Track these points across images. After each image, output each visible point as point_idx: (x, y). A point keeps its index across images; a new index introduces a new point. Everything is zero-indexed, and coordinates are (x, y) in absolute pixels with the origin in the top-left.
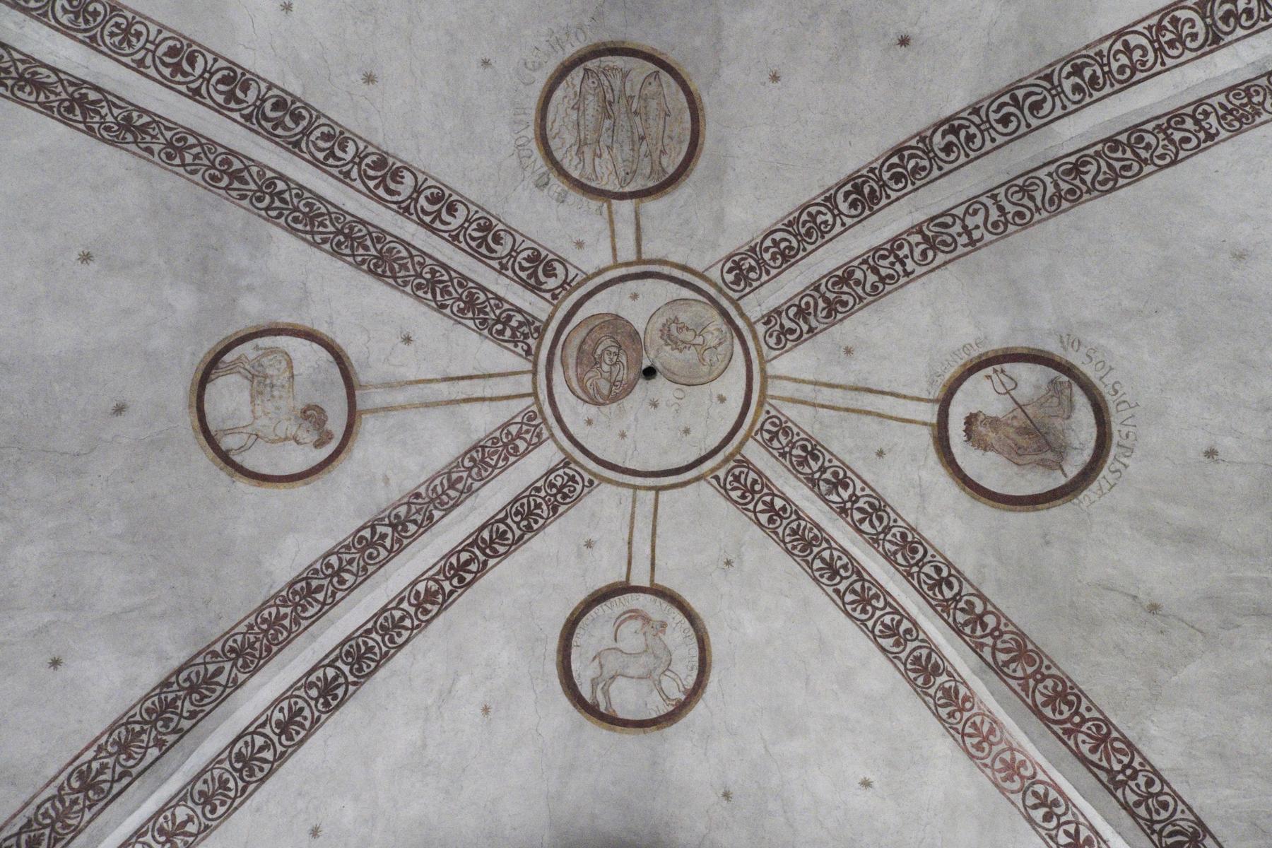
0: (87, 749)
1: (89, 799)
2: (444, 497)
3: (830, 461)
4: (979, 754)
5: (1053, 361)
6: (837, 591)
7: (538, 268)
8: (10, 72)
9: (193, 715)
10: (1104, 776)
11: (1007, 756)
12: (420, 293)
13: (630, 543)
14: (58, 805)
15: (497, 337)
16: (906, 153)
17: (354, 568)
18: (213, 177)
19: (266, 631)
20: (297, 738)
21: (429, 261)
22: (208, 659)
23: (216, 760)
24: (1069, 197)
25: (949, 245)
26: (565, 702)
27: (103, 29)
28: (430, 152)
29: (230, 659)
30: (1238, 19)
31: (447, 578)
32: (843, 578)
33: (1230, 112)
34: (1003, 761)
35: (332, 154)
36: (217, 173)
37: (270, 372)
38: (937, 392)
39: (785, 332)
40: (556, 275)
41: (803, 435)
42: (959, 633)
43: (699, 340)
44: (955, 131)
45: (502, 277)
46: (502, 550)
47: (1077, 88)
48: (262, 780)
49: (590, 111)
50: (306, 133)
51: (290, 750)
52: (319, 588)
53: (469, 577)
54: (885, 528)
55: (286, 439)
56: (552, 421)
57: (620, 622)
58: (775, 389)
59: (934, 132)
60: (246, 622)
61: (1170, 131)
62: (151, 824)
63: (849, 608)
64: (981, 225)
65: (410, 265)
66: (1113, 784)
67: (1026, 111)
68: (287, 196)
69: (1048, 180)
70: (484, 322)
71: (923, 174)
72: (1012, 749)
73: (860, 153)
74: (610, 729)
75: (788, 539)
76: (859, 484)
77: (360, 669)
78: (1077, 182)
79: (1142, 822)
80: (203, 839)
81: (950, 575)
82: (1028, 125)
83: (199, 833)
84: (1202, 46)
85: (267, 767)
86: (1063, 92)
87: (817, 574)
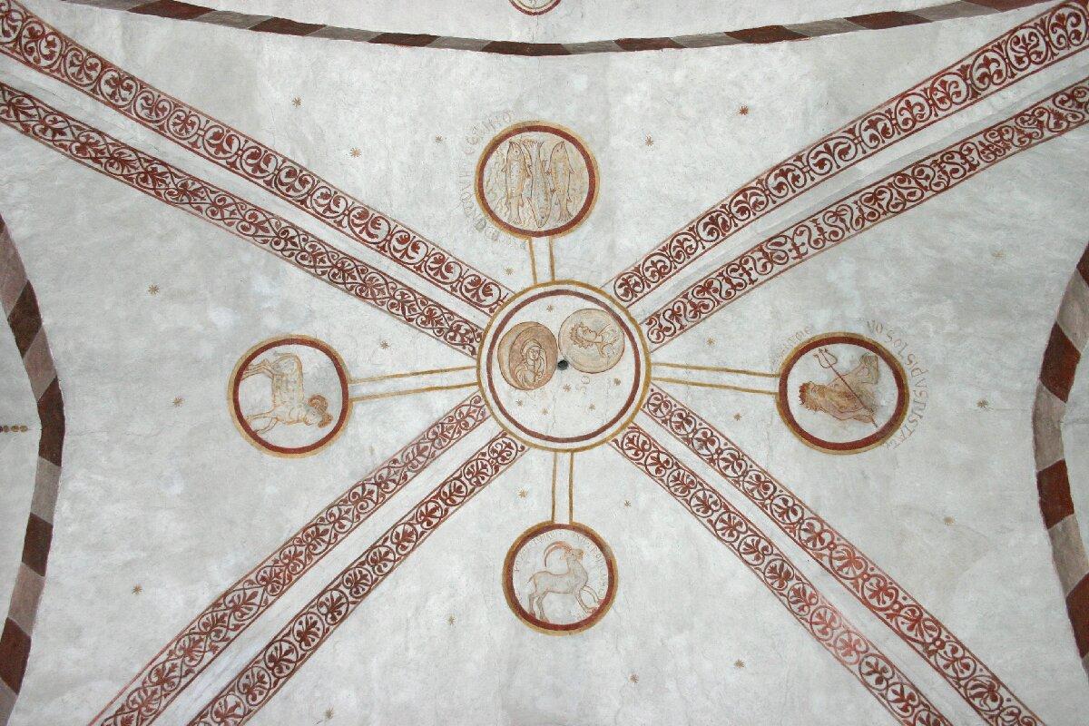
0: (162, 653)
1: (165, 690)
2: (415, 462)
3: (700, 424)
4: (826, 637)
5: (863, 341)
6: (710, 521)
7: (478, 289)
8: (103, 153)
9: (237, 627)
11: (845, 637)
12: (394, 310)
13: (553, 492)
14: (143, 694)
16: (748, 192)
17: (350, 516)
18: (244, 228)
19: (287, 565)
20: (313, 644)
21: (399, 286)
22: (246, 586)
23: (255, 661)
24: (870, 218)
25: (783, 259)
27: (168, 121)
28: (399, 208)
29: (262, 586)
30: (991, 78)
31: (418, 523)
32: (713, 511)
33: (987, 148)
34: (842, 641)
35: (329, 209)
36: (247, 225)
37: (285, 371)
38: (778, 369)
39: (662, 329)
40: (492, 295)
41: (679, 406)
42: (804, 547)
43: (599, 339)
44: (784, 174)
45: (453, 297)
46: (459, 500)
47: (873, 138)
48: (289, 676)
49: (515, 173)
50: (310, 194)
51: (308, 653)
52: (326, 532)
53: (435, 521)
54: (743, 472)
55: (298, 421)
56: (492, 403)
57: (548, 551)
59: (769, 176)
60: (273, 558)
61: (943, 165)
62: (210, 708)
63: (720, 533)
64: (806, 242)
65: (386, 290)
66: (928, 653)
67: (836, 156)
68: (296, 240)
69: (854, 207)
70: (441, 330)
71: (762, 207)
72: (848, 632)
73: (713, 196)
74: (544, 632)
75: (671, 484)
76: (723, 441)
77: (357, 592)
78: (876, 207)
79: (951, 680)
80: (248, 720)
81: (794, 505)
82: (838, 167)
83: (245, 715)
84: (965, 100)
85: (292, 666)
86: (863, 141)
87: (694, 509)
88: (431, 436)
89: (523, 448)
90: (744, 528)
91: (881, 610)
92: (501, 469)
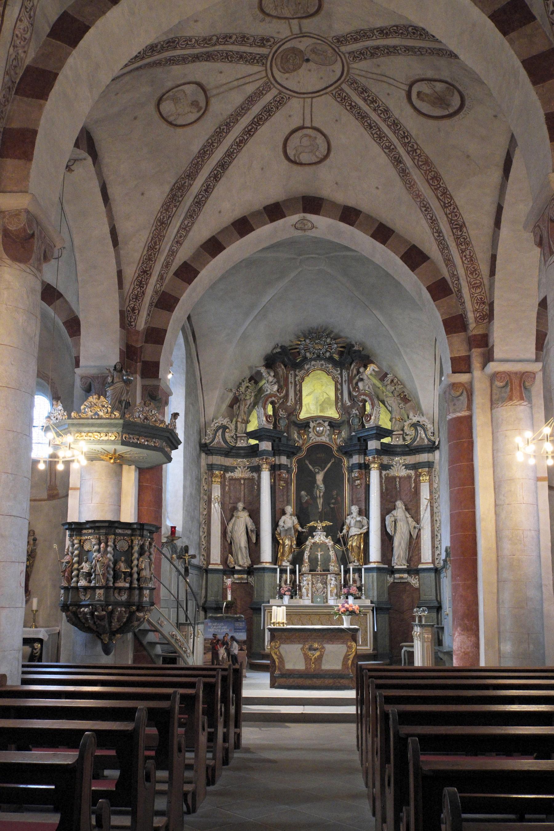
6: (372, 133)
9: (181, 196)
10: (442, 204)
11: (417, 192)
15: (252, 64)
23: (191, 206)
26: (286, 162)
35: (187, 44)
42: (408, 153)
46: (261, 123)
48: (204, 205)
52: (207, 150)
53: (252, 133)
55: (188, 113)
56: (273, 82)
57: (301, 138)
58: (352, 71)
66: (444, 207)
88: (247, 102)
89: (289, 98)
90: (385, 139)
91: (432, 185)
92: (280, 108)
